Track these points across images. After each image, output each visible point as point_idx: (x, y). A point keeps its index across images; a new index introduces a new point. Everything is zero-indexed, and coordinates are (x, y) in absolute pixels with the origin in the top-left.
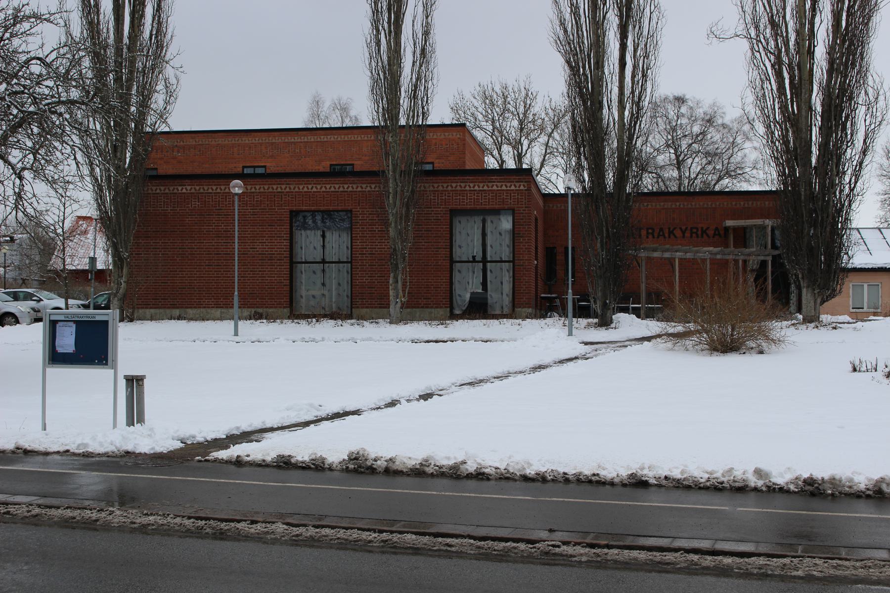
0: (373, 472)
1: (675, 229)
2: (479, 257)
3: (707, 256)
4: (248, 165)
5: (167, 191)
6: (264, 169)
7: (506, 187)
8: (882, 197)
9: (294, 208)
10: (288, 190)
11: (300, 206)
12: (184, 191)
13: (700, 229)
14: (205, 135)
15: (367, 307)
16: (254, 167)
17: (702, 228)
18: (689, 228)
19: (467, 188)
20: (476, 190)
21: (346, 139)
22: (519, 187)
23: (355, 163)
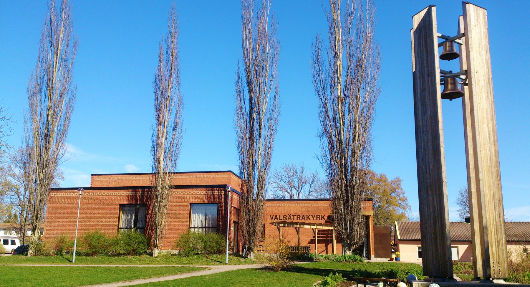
1: (310, 215)
8: (460, 212)
9: (121, 203)
10: (119, 194)
11: (124, 202)
13: (321, 216)
17: (322, 216)
18: (316, 215)
19: (198, 194)
20: (201, 195)
21: (181, 177)
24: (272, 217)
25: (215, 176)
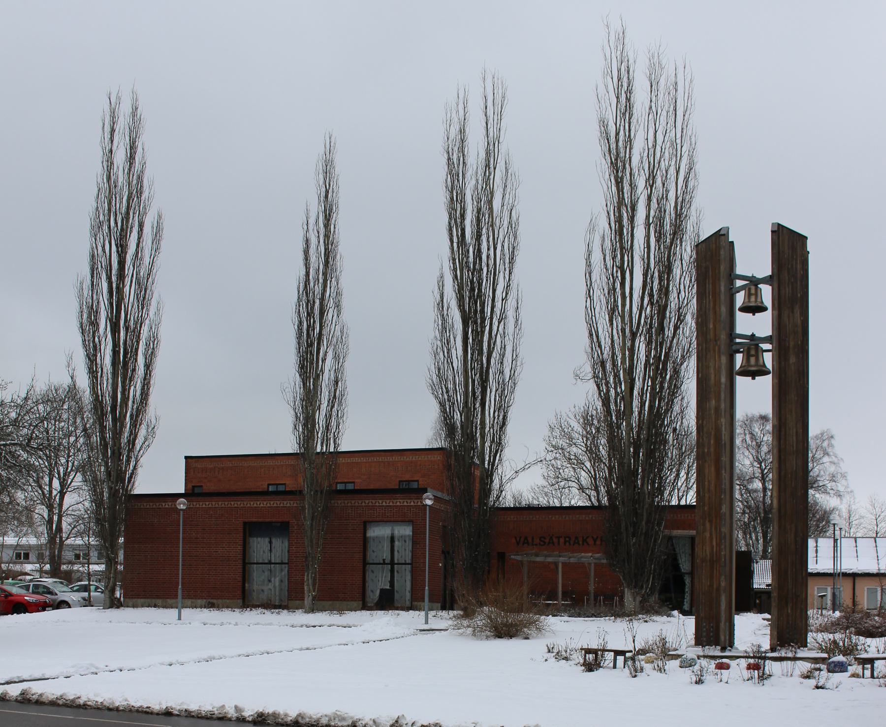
0: (29, 703)
1: (588, 537)
2: (388, 560)
3: (591, 560)
4: (272, 483)
5: (154, 506)
6: (284, 486)
7: (407, 503)
9: (246, 520)
10: (242, 505)
12: (167, 506)
14: (240, 458)
15: (299, 600)
16: (277, 485)
19: (377, 504)
22: (417, 503)
23: (356, 481)
24: (518, 539)
25: (414, 459)
